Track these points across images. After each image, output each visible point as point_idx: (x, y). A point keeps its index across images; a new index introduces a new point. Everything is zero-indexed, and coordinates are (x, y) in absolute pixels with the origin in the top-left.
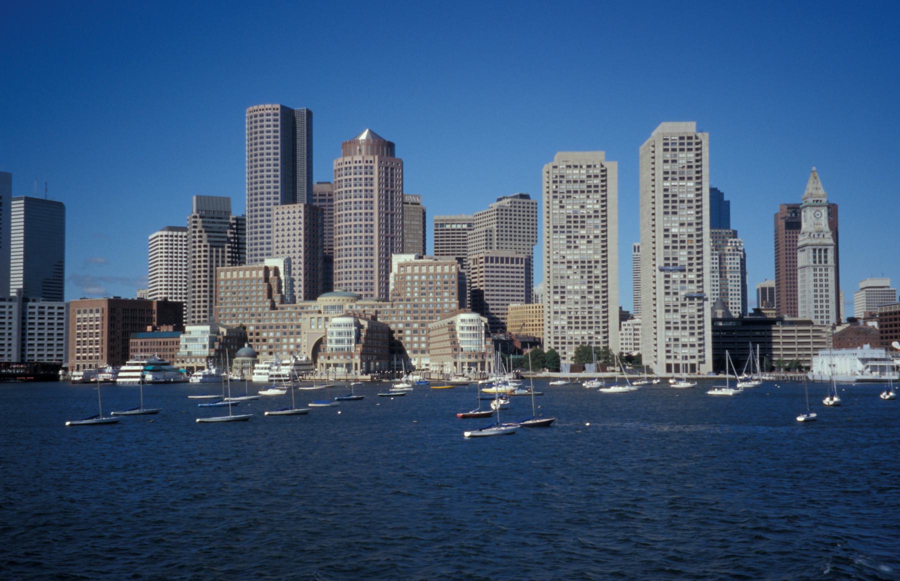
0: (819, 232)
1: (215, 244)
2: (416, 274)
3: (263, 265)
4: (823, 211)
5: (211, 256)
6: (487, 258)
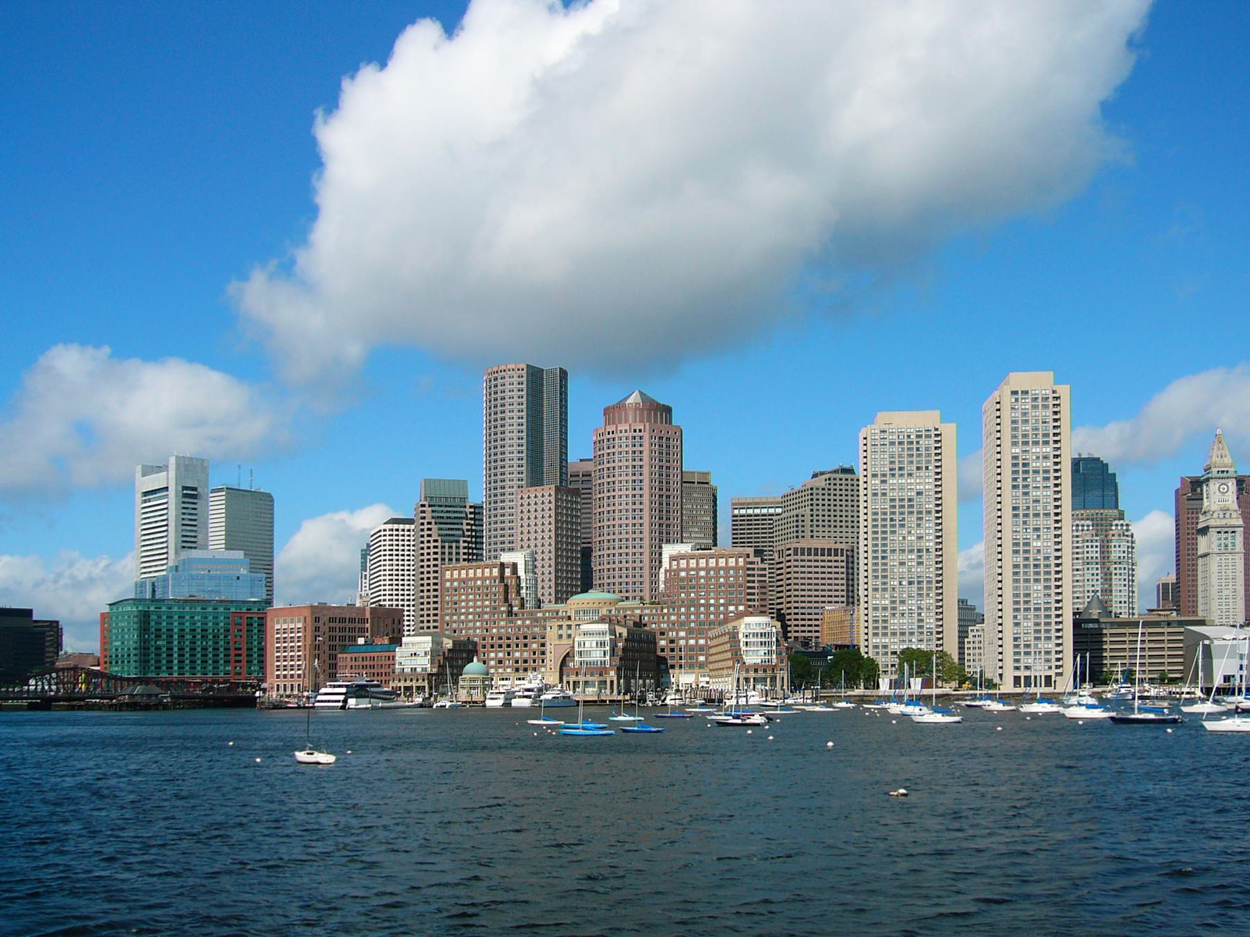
0: (1225, 510)
1: (449, 539)
2: (702, 569)
3: (498, 562)
4: (1230, 484)
5: (443, 553)
6: (795, 550)
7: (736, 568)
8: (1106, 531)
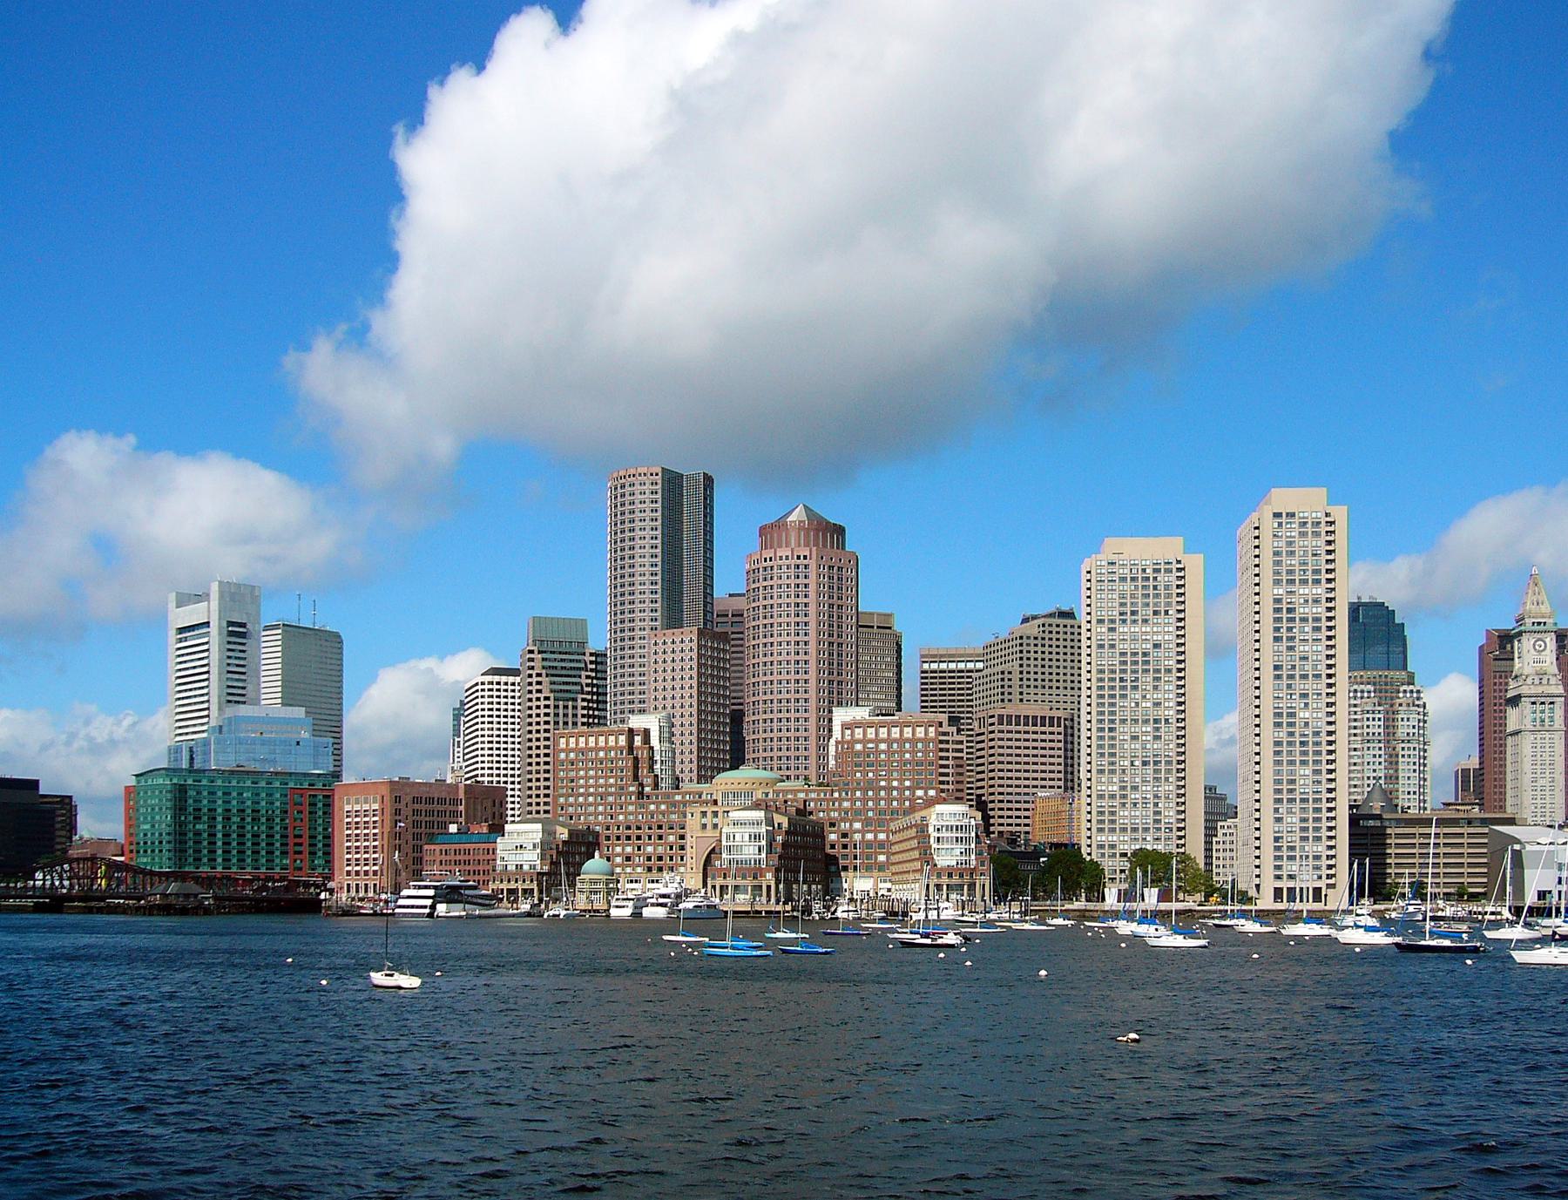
0: (1541, 674)
1: (564, 696)
2: (883, 741)
4: (1548, 640)
5: (557, 715)
7: (925, 741)
8: (1392, 699)
